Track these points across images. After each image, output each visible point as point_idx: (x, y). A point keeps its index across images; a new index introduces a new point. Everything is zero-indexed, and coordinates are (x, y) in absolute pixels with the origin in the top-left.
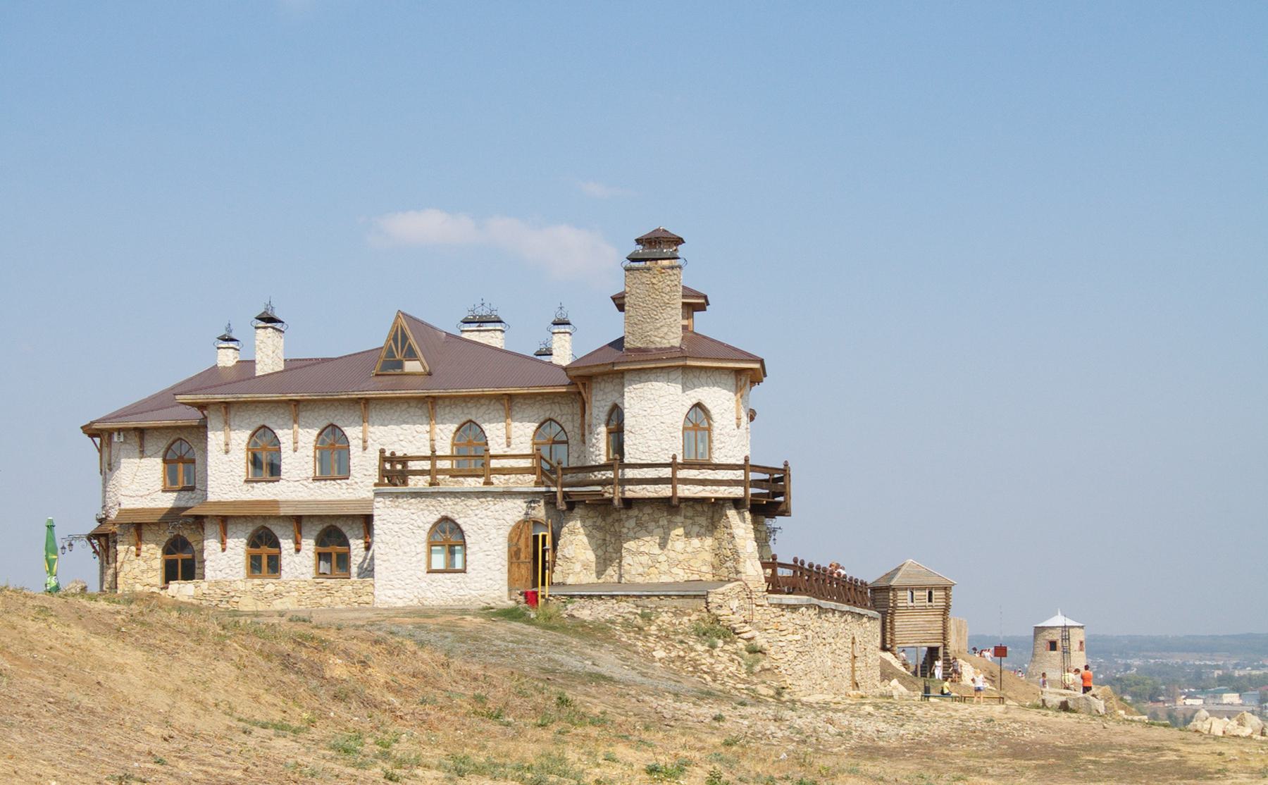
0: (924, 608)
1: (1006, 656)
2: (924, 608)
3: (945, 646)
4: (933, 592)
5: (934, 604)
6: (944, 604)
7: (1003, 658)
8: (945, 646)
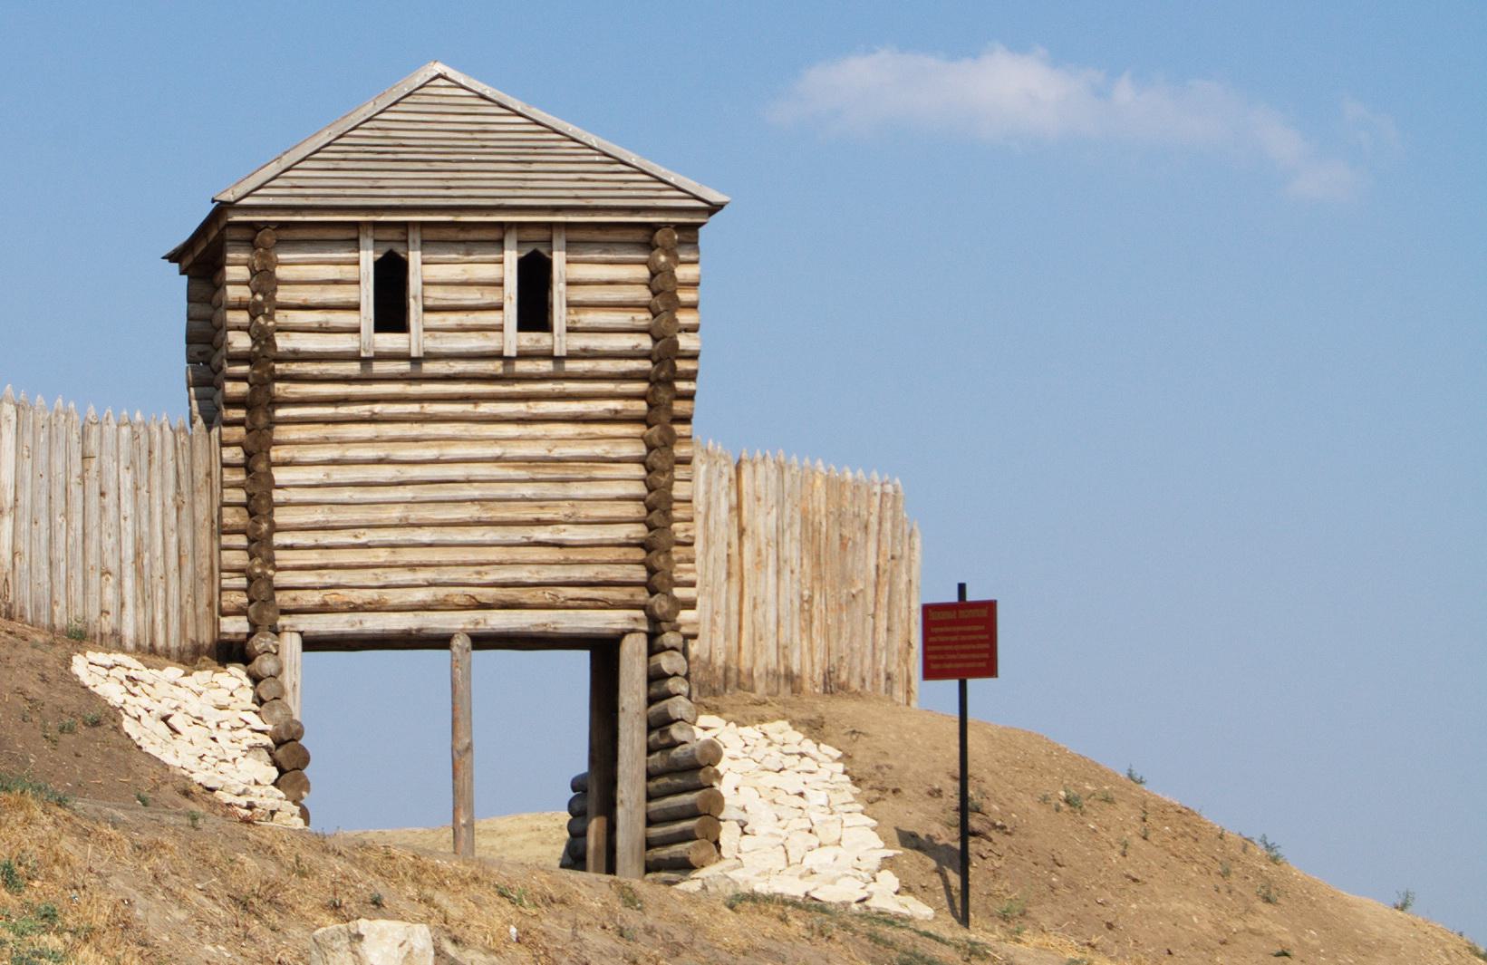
0: (495, 367)
1: (989, 669)
2: (495, 367)
3: (656, 628)
4: (558, 258)
5: (559, 341)
6: (645, 342)
7: (972, 683)
8: (656, 628)
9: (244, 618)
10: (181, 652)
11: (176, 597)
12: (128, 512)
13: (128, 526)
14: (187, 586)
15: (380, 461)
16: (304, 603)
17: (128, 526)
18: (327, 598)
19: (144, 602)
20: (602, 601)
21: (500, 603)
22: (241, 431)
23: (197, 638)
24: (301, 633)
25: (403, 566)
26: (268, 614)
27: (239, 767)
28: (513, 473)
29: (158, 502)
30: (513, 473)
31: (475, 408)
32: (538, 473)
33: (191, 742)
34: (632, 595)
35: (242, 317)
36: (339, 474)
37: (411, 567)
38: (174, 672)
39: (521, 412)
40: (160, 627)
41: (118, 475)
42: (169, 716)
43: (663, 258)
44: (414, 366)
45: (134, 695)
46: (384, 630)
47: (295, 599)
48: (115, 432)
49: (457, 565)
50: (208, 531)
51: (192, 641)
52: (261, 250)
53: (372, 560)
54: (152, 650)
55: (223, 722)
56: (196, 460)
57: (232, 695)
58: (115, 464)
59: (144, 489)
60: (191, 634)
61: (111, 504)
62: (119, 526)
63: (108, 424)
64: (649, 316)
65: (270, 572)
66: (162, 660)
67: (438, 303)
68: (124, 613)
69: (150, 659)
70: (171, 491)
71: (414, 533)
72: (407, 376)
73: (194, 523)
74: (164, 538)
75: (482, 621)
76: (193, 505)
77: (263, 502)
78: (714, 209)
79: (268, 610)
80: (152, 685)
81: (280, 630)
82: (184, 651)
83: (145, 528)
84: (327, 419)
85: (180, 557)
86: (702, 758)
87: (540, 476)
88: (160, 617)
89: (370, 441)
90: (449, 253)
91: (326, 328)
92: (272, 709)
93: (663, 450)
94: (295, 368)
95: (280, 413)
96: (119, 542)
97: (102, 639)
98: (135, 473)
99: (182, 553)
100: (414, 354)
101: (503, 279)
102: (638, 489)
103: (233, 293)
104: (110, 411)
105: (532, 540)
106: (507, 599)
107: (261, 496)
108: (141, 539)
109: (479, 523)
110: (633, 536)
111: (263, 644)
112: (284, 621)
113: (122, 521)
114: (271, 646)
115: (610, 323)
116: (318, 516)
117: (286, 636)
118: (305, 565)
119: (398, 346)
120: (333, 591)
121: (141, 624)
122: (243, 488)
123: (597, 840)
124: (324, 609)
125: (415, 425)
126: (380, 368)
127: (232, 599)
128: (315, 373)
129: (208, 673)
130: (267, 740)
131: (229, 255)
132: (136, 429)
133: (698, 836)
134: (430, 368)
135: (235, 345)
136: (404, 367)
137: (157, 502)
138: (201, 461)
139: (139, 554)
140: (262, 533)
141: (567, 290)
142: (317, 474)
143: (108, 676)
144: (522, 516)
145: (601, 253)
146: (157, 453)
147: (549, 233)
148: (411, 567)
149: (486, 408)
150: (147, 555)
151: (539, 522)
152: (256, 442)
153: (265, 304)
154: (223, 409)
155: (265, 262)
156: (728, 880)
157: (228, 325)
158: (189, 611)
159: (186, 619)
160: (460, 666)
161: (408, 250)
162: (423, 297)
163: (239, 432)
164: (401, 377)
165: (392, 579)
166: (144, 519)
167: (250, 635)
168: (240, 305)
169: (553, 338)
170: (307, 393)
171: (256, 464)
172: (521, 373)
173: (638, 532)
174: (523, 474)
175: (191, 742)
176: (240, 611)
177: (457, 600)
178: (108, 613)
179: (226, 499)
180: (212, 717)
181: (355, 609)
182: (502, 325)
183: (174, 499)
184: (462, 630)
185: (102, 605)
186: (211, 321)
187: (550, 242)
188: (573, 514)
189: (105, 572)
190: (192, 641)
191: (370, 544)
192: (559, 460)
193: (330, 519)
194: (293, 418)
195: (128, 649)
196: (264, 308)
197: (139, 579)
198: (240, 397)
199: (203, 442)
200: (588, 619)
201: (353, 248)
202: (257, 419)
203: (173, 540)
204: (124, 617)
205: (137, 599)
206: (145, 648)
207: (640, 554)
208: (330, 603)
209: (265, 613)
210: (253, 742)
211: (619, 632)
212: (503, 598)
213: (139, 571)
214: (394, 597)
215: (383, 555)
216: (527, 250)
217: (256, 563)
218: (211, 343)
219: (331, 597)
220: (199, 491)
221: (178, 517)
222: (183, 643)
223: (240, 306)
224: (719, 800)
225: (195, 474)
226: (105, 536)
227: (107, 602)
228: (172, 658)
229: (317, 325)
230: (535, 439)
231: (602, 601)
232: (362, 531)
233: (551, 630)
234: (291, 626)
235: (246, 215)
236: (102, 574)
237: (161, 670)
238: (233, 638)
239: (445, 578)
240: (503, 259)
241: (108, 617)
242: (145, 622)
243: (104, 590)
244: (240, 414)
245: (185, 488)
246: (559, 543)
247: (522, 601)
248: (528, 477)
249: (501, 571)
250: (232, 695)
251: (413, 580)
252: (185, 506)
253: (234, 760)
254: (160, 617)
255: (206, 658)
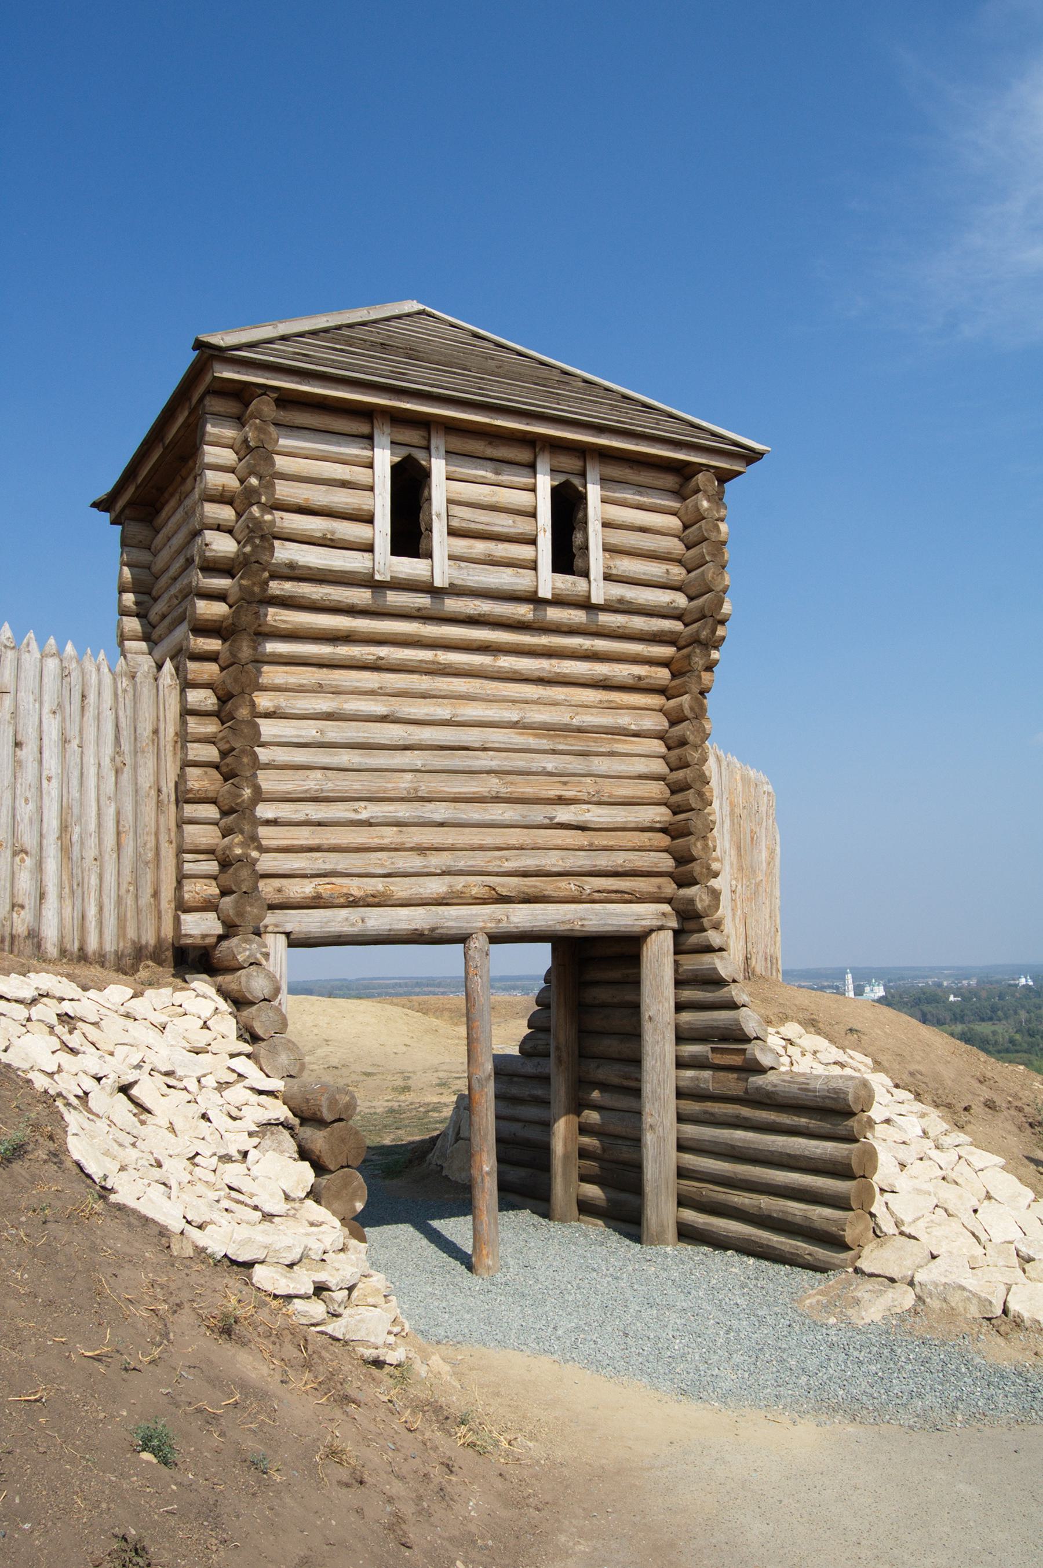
0: (524, 611)
2: (524, 611)
9: (213, 915)
10: (119, 956)
11: (114, 884)
12: (53, 770)
13: (52, 789)
14: (127, 870)
15: (384, 719)
16: (292, 895)
17: (52, 789)
18: (321, 889)
19: (73, 892)
20: (629, 893)
21: (522, 895)
22: (213, 668)
23: (139, 937)
24: (288, 934)
25: (412, 849)
26: (252, 910)
27: (255, 1170)
28: (532, 742)
29: (92, 761)
30: (532, 742)
31: (495, 660)
32: (560, 743)
33: (172, 1129)
34: (659, 887)
35: (226, 513)
36: (334, 732)
37: (422, 850)
38: (118, 992)
39: (543, 669)
40: (93, 923)
41: (41, 722)
42: (131, 1085)
43: (705, 504)
44: (434, 600)
45: (73, 1051)
46: (390, 930)
47: (279, 891)
48: (38, 664)
49: (473, 849)
50: (154, 801)
51: (134, 942)
52: (258, 421)
53: (376, 842)
54: (83, 957)
55: (204, 1076)
56: (140, 713)
57: (205, 1026)
58: (37, 705)
59: (75, 742)
60: (131, 933)
61: (31, 759)
62: (40, 789)
63: (29, 651)
64: (684, 571)
65: (254, 854)
66: (95, 971)
67: (465, 525)
68: (43, 906)
69: (81, 970)
70: (108, 750)
71: (425, 809)
72: (424, 613)
73: (137, 791)
74: (99, 809)
75: (504, 918)
76: (135, 768)
77: (245, 760)
78: (751, 457)
79: (251, 905)
80: (95, 1024)
81: (262, 929)
82: (122, 955)
83: (75, 793)
84: (321, 661)
85: (118, 834)
86: (855, 1102)
87: (561, 747)
88: (92, 911)
89: (372, 693)
90: (476, 468)
91: (331, 540)
92: (273, 1051)
93: (695, 722)
94: (288, 587)
95: (272, 647)
96: (40, 810)
97: (12, 943)
98: (64, 720)
99: (121, 828)
100: (438, 583)
101: (536, 508)
102: (658, 767)
103: (214, 479)
104: (32, 635)
105: (556, 821)
106: (530, 891)
107: (243, 751)
108: (70, 807)
109: (497, 799)
110: (658, 819)
111: (247, 953)
112: (271, 918)
113: (45, 782)
114: (259, 956)
115: (644, 574)
116: (312, 782)
117: (269, 939)
118: (293, 846)
119: (418, 572)
120: (327, 880)
121: (68, 922)
122: (214, 743)
123: (565, 1145)
124: (316, 903)
125: (424, 677)
126: (395, 599)
127: (198, 888)
128: (315, 597)
129: (167, 991)
130: (282, 1112)
131: (209, 428)
132: (65, 664)
133: (854, 1207)
134: (453, 605)
135: (214, 547)
136: (422, 601)
137: (90, 760)
138: (147, 715)
139: (66, 827)
140: (243, 801)
141: (603, 532)
142: (309, 730)
143: (29, 1020)
144: (544, 792)
145: (634, 494)
146: (92, 698)
147: (580, 463)
148: (422, 850)
149: (506, 662)
150: (77, 829)
151: (561, 801)
152: (236, 680)
153: (262, 490)
154: (191, 637)
155: (262, 436)
156: (966, 1294)
157: (206, 521)
158: (129, 903)
159: (125, 915)
160: (479, 973)
161: (430, 457)
162: (448, 516)
163: (210, 670)
164: (417, 614)
165: (400, 866)
166: (75, 782)
167: (221, 938)
168: (222, 495)
169: (589, 582)
170: (301, 623)
171: (237, 709)
172: (551, 622)
173: (662, 815)
174: (544, 744)
175: (172, 1129)
176: (208, 906)
177: (474, 891)
178: (22, 907)
179: (191, 756)
180: (190, 1067)
181: (354, 903)
182: (535, 562)
183: (113, 760)
184: (481, 929)
185: (13, 895)
186: (149, 568)
187: (583, 475)
188: (598, 792)
189: (20, 851)
190: (134, 942)
191: (372, 821)
192: (580, 730)
193: (325, 788)
194: (281, 655)
195: (49, 955)
196: (260, 495)
197: (65, 860)
198: (215, 621)
199: (149, 691)
200: (617, 915)
201: (367, 446)
202: (240, 649)
203: (110, 811)
204: (44, 913)
205: (62, 888)
206: (72, 954)
207: (664, 840)
208: (324, 895)
209: (248, 909)
210: (264, 1116)
211: (647, 930)
212: (526, 889)
213: (65, 850)
214: (401, 888)
215: (389, 836)
216: (561, 479)
217: (236, 840)
218: (150, 594)
219: (324, 887)
220: (143, 752)
221: (116, 783)
222: (121, 944)
223: (223, 498)
224: (870, 1156)
225: (138, 732)
226: (20, 802)
227: (21, 892)
228: (107, 964)
229: (319, 535)
230: (555, 704)
231: (629, 893)
232: (363, 804)
233: (578, 927)
234: (276, 926)
235: (238, 372)
236: (15, 854)
237: (100, 990)
238: (199, 941)
239: (461, 865)
240: (535, 485)
241: (22, 912)
242: (73, 917)
243: (17, 876)
244: (213, 644)
245: (126, 746)
246: (582, 824)
247: (546, 893)
248: (548, 748)
249: (523, 858)
250: (205, 1026)
251: (425, 867)
252: (127, 769)
253: (245, 1154)
254: (92, 911)
255: (150, 963)
